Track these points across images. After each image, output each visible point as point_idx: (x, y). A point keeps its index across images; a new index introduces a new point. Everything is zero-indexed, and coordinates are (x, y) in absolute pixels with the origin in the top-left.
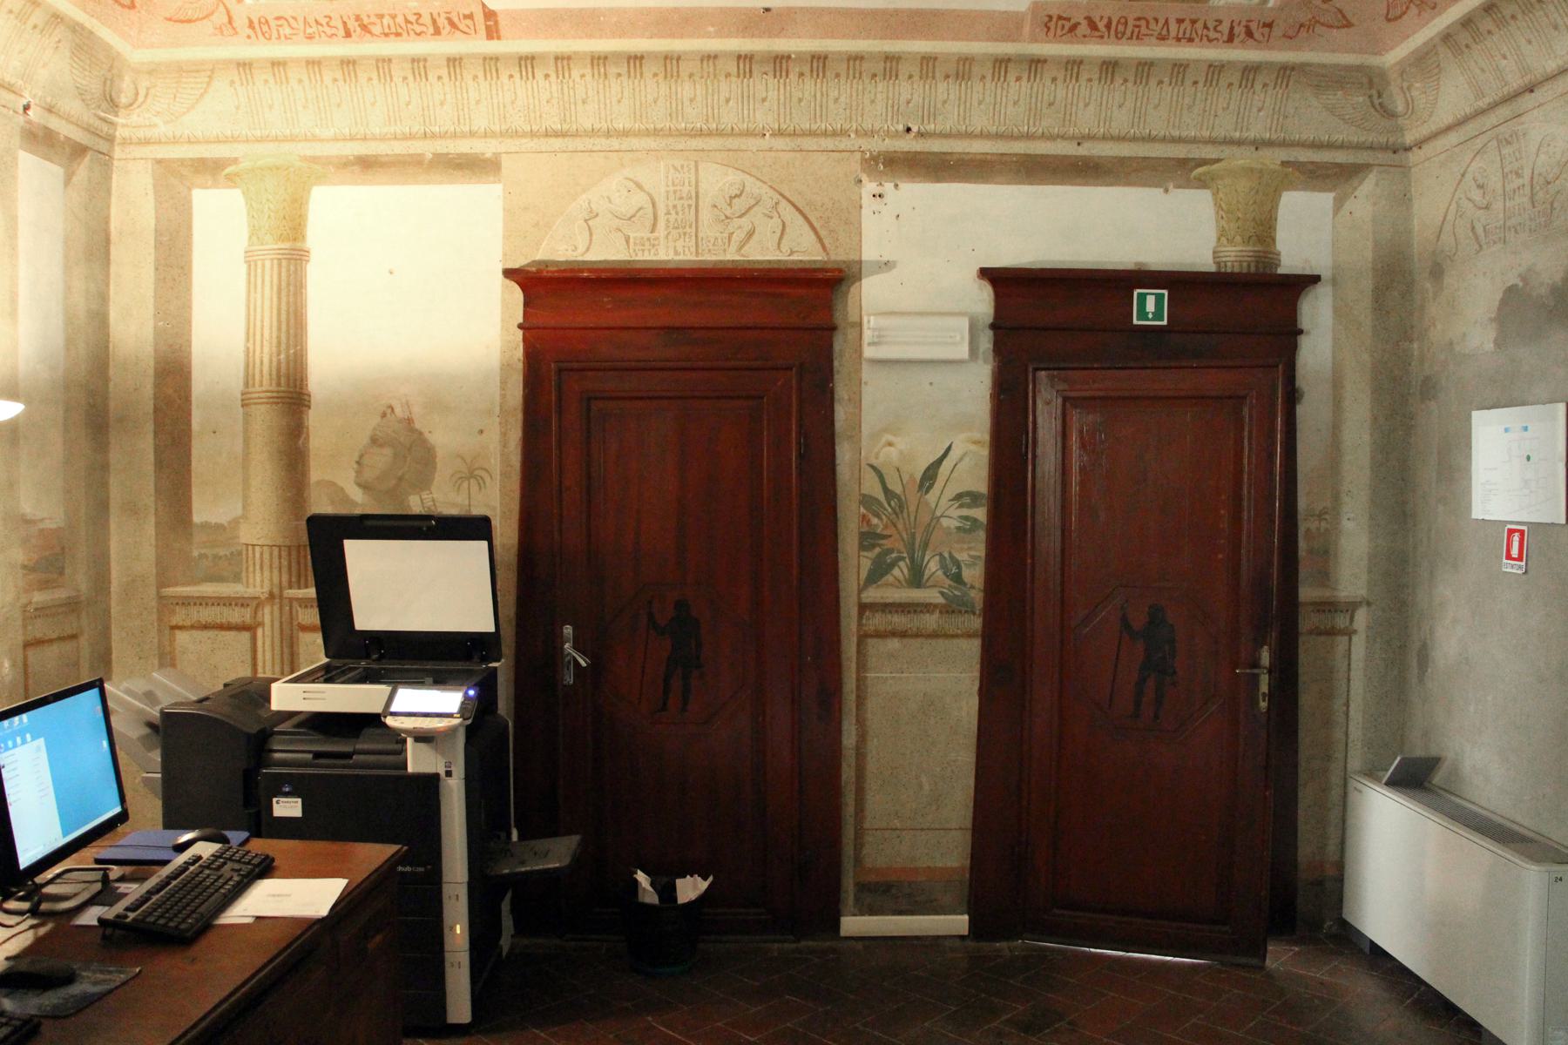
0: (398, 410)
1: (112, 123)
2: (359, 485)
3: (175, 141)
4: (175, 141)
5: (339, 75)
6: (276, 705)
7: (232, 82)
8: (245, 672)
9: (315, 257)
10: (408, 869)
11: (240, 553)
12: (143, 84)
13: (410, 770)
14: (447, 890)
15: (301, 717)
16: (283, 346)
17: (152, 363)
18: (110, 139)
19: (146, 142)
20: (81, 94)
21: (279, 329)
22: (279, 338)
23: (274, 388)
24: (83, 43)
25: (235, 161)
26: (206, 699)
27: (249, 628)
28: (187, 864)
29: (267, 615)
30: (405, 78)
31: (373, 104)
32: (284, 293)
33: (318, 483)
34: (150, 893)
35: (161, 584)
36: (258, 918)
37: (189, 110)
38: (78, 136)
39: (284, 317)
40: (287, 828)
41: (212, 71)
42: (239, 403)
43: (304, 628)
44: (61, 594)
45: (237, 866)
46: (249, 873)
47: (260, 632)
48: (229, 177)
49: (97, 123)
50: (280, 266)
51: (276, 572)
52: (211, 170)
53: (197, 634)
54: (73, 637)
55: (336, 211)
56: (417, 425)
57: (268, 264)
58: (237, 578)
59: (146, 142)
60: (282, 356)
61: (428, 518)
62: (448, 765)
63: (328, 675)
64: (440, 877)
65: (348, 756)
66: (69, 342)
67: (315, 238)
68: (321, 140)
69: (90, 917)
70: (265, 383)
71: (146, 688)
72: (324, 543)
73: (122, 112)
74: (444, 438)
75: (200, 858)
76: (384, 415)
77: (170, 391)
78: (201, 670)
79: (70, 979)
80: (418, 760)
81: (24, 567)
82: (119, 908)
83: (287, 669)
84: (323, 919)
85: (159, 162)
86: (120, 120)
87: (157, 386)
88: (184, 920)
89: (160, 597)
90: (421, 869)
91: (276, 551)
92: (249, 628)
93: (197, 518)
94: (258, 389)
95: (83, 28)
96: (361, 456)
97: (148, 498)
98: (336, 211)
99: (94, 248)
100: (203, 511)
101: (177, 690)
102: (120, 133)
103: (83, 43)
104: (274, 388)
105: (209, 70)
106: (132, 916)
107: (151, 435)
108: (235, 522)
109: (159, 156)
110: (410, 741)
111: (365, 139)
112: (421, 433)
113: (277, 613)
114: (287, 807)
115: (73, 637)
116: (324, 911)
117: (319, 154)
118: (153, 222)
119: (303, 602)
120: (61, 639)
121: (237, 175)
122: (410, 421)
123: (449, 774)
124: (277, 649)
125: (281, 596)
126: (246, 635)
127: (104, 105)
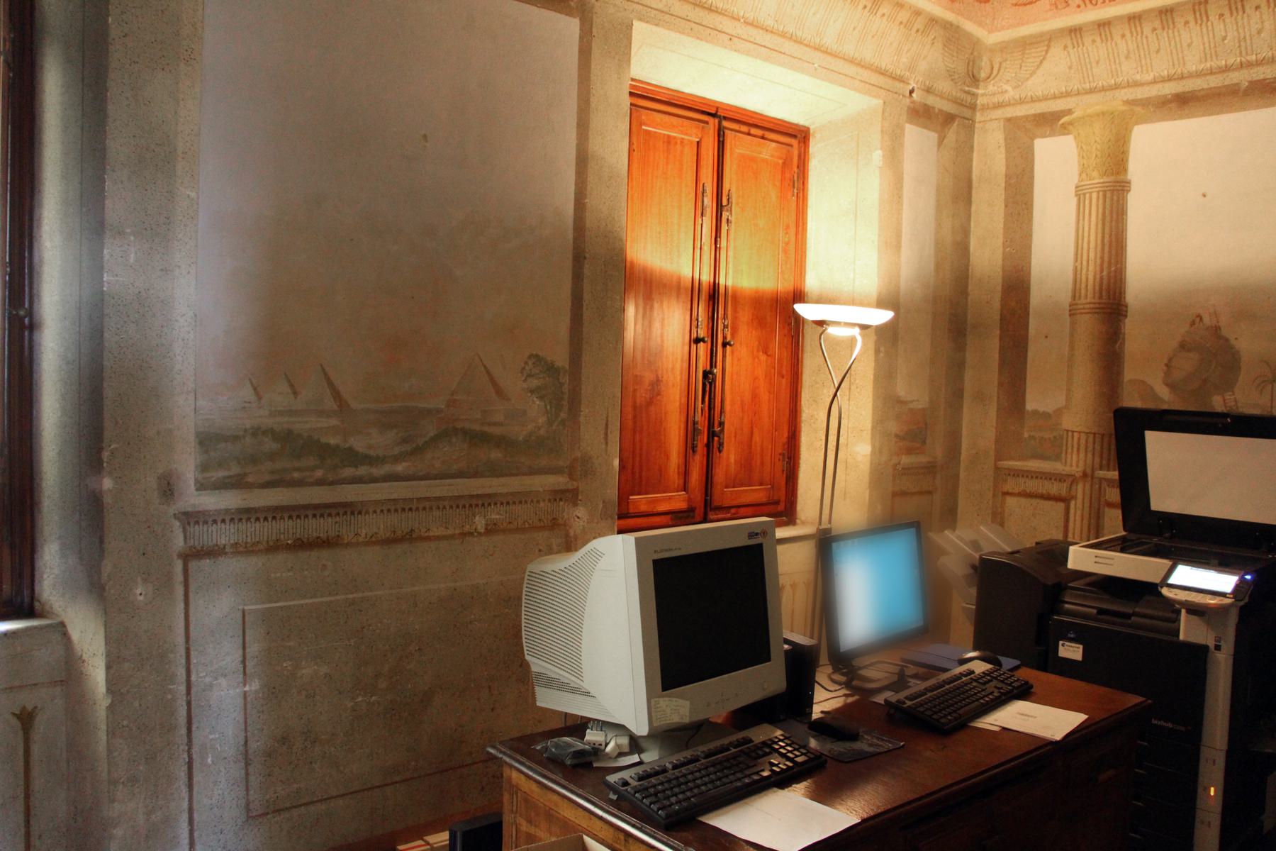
0: (1206, 319)
1: (973, 94)
2: (1167, 385)
3: (1021, 101)
4: (1021, 101)
5: (1157, 23)
6: (1071, 565)
7: (1066, 47)
8: (1060, 537)
9: (1135, 187)
10: (1170, 725)
11: (1061, 437)
12: (997, 60)
13: (1181, 637)
14: (1205, 753)
15: (1093, 578)
16: (1106, 265)
17: (1000, 281)
18: (973, 107)
19: (1000, 106)
20: (951, 75)
21: (1103, 249)
22: (1102, 258)
23: (1097, 300)
24: (952, 36)
25: (1069, 112)
26: (1018, 552)
27: (1065, 500)
28: (962, 675)
29: (1080, 489)
30: (1221, 15)
31: (1189, 45)
32: (1108, 219)
33: (1130, 381)
34: (927, 690)
35: (999, 458)
36: (1004, 729)
37: (1031, 75)
38: (947, 107)
39: (1107, 240)
40: (1067, 668)
41: (1050, 40)
42: (1067, 313)
43: (1110, 505)
44: (923, 459)
45: (1000, 685)
46: (1011, 691)
47: (1073, 503)
48: (1064, 126)
49: (963, 96)
50: (1105, 196)
51: (1090, 455)
52: (1049, 122)
53: (1023, 501)
54: (930, 493)
55: (1153, 144)
56: (1225, 332)
57: (1094, 195)
58: (1057, 458)
59: (1000, 106)
60: (1105, 273)
61: (1223, 415)
62: (1218, 639)
63: (1123, 545)
64: (1200, 739)
65: (1128, 616)
66: (938, 266)
67: (1135, 169)
68: (1142, 85)
69: (880, 699)
70: (1089, 297)
71: (972, 537)
72: (1127, 433)
73: (982, 85)
74: (1247, 343)
75: (973, 672)
76: (1193, 323)
77: (1013, 304)
78: (1022, 527)
79: (854, 737)
80: (1189, 631)
81: (897, 436)
82: (901, 695)
83: (1084, 536)
84: (1057, 742)
85: (1009, 120)
86: (980, 91)
87: (1003, 299)
88: (945, 716)
89: (997, 469)
90: (1183, 728)
91: (1091, 437)
92: (1065, 500)
93: (1030, 406)
94: (1083, 301)
95: (951, 24)
96: (1170, 360)
97: (993, 390)
98: (1153, 144)
99: (959, 192)
100: (1033, 403)
101: (996, 542)
102: (980, 101)
103: (952, 36)
104: (1097, 300)
105: (1048, 39)
106: (909, 703)
107: (997, 340)
108: (1059, 412)
109: (1009, 116)
110: (1183, 611)
111: (1182, 77)
112: (1227, 340)
113: (1088, 491)
114: (1071, 651)
115: (930, 493)
116: (1058, 736)
117: (1139, 97)
118: (1003, 169)
119: (1109, 481)
120: (921, 493)
121: (1070, 123)
122: (1217, 328)
123: (1218, 648)
124: (1086, 521)
125: (1092, 477)
126: (1061, 505)
127: (968, 80)
